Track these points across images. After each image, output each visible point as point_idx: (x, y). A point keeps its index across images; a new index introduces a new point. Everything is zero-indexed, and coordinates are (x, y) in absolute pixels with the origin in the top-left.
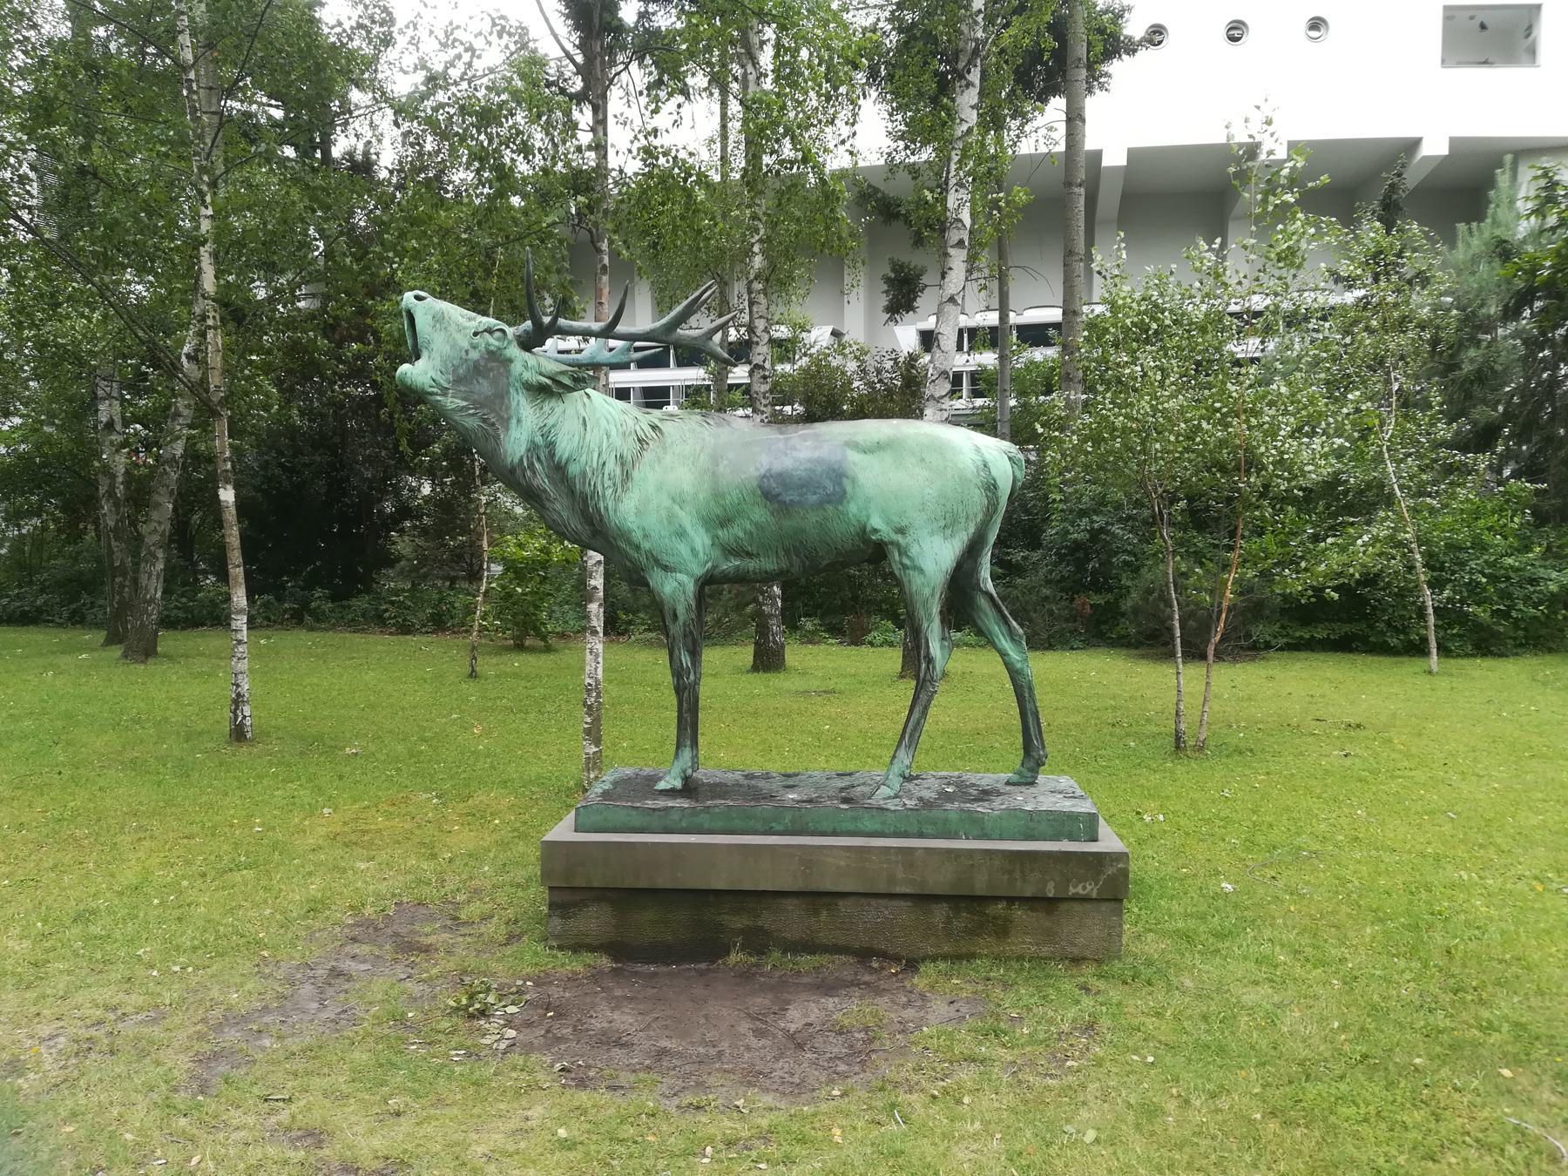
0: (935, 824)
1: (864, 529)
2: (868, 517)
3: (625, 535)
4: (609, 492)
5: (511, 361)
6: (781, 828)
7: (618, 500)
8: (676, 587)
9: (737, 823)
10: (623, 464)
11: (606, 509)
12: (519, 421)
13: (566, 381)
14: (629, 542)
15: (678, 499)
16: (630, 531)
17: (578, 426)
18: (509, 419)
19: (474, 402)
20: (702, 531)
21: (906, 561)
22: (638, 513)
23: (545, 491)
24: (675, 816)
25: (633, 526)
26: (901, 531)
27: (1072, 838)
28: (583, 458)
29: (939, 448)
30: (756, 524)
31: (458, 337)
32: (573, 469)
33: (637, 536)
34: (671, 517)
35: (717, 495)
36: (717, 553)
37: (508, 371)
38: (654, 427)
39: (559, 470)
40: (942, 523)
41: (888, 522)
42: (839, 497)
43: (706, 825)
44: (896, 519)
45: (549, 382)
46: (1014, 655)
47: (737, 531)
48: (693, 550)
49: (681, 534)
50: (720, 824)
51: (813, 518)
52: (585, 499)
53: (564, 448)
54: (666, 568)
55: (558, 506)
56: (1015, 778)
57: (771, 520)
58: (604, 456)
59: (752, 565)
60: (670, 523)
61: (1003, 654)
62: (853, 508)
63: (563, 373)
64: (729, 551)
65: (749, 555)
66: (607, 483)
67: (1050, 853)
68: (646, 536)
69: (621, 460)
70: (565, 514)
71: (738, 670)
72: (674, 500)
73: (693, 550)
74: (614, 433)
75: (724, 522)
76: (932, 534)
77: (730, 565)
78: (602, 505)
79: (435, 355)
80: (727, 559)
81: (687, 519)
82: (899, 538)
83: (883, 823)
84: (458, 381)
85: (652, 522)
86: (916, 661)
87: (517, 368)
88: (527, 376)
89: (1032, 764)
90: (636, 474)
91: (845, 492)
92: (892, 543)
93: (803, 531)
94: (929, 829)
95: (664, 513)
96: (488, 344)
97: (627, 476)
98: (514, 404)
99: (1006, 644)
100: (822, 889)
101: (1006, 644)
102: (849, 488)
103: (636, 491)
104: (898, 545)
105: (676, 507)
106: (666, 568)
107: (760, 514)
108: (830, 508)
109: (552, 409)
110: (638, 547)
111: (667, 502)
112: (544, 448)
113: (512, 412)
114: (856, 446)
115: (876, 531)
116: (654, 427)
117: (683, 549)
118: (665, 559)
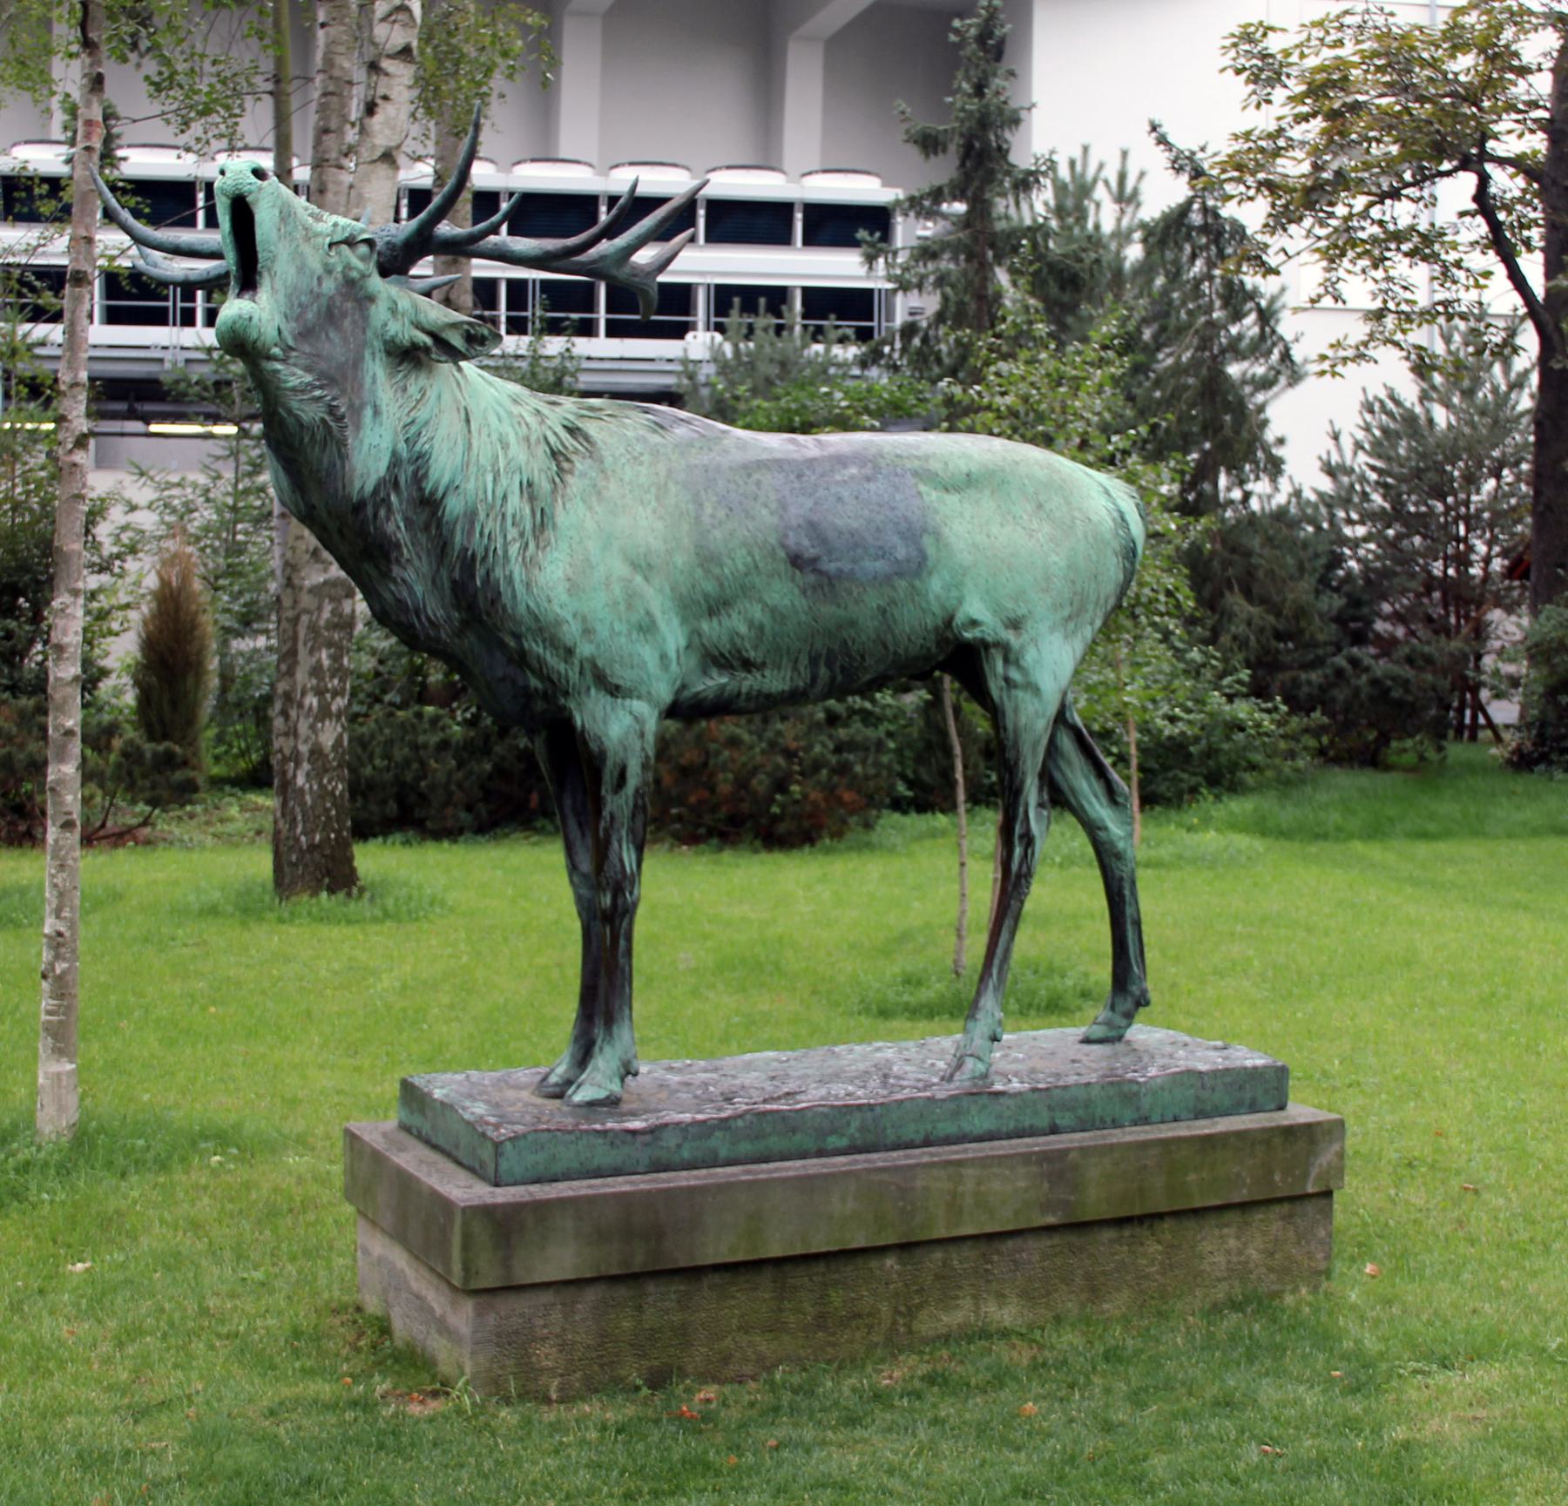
0: (1073, 1109)
1: (949, 622)
2: (960, 601)
3: (547, 632)
4: (514, 550)
5: (371, 299)
6: (844, 1142)
7: (529, 564)
8: (623, 727)
9: (775, 1143)
10: (532, 499)
11: (510, 580)
12: (377, 412)
13: (457, 341)
14: (553, 642)
15: (642, 565)
16: (558, 622)
17: (459, 425)
18: (362, 406)
19: (321, 375)
20: (676, 622)
21: (1015, 675)
22: (574, 588)
23: (398, 546)
24: (670, 1140)
25: (566, 614)
26: (1015, 624)
27: (1254, 1108)
28: (471, 486)
29: (1062, 488)
30: (773, 611)
31: (307, 249)
32: (454, 506)
33: (571, 631)
34: (631, 597)
35: (707, 559)
36: (692, 661)
37: (366, 318)
38: (573, 431)
39: (429, 505)
40: (1066, 612)
41: (997, 609)
42: (918, 567)
43: (723, 1153)
44: (1010, 605)
45: (428, 340)
46: (1115, 828)
47: (735, 625)
48: (663, 657)
49: (647, 628)
50: (745, 1148)
51: (873, 600)
52: (468, 563)
53: (442, 469)
54: (614, 691)
55: (410, 575)
56: (1099, 1031)
57: (801, 603)
58: (504, 481)
59: (748, 682)
60: (629, 607)
61: (1092, 829)
62: (936, 585)
63: (454, 326)
64: (715, 659)
65: (748, 665)
66: (512, 533)
67: (1241, 1135)
68: (587, 632)
69: (528, 488)
70: (419, 589)
71: (246, 909)
72: (635, 566)
73: (663, 657)
74: (512, 439)
75: (716, 607)
76: (1052, 630)
77: (713, 683)
78: (498, 573)
79: (279, 284)
80: (705, 672)
81: (656, 600)
82: (1009, 636)
83: (999, 1117)
84: (305, 334)
85: (597, 605)
86: (1013, 835)
87: (379, 312)
88: (394, 328)
89: (1128, 1004)
90: (561, 518)
91: (923, 557)
92: (997, 644)
93: (853, 623)
94: (1064, 1120)
95: (617, 589)
96: (348, 267)
97: (542, 523)
98: (368, 380)
99: (1100, 810)
100: (854, 1245)
101: (1100, 810)
102: (931, 551)
103: (564, 545)
104: (1005, 648)
105: (639, 579)
106: (614, 691)
107: (783, 593)
108: (903, 584)
109: (423, 392)
110: (570, 652)
111: (620, 569)
112: (410, 471)
113: (366, 395)
114: (925, 475)
115: (974, 623)
116: (573, 431)
117: (648, 654)
118: (621, 675)
